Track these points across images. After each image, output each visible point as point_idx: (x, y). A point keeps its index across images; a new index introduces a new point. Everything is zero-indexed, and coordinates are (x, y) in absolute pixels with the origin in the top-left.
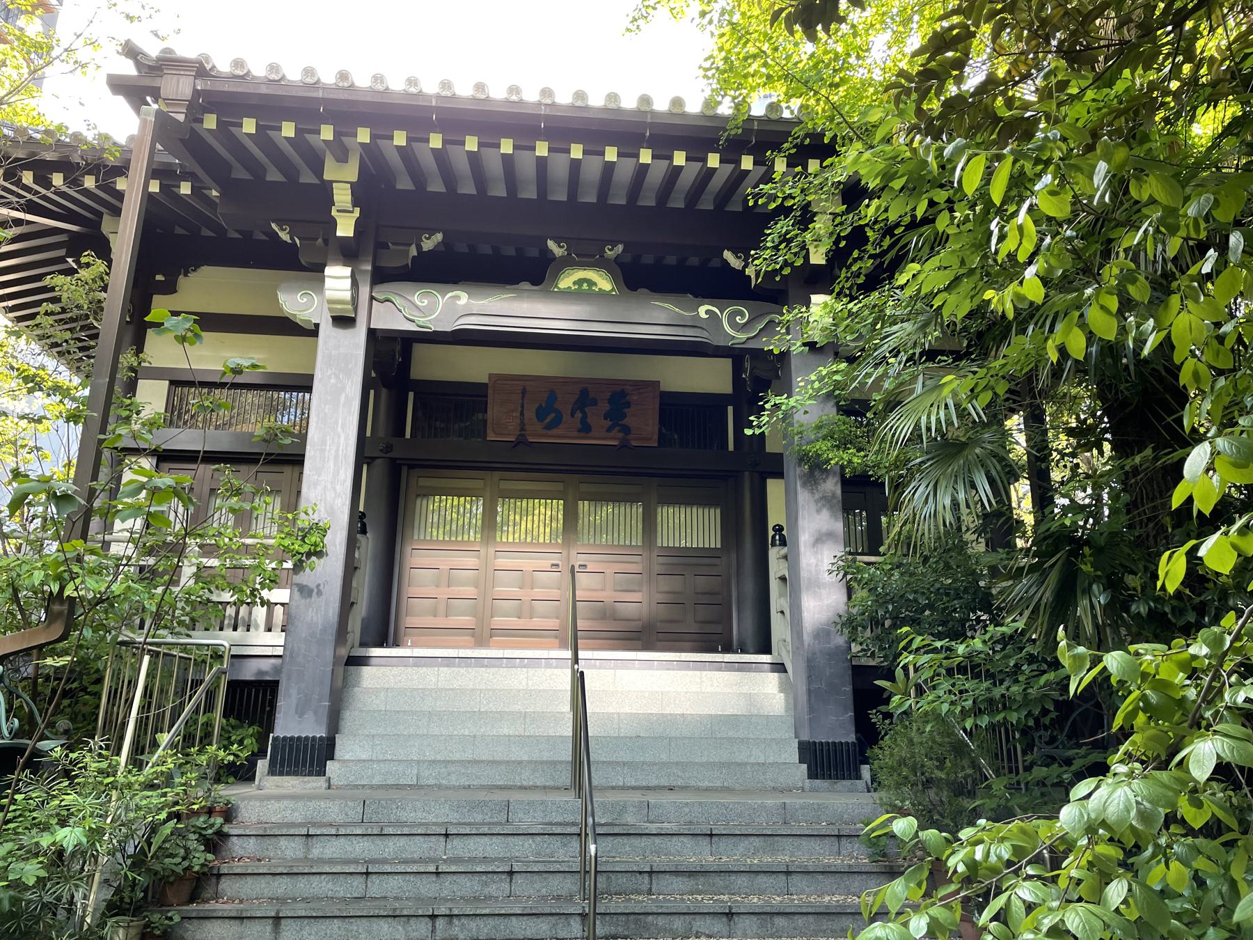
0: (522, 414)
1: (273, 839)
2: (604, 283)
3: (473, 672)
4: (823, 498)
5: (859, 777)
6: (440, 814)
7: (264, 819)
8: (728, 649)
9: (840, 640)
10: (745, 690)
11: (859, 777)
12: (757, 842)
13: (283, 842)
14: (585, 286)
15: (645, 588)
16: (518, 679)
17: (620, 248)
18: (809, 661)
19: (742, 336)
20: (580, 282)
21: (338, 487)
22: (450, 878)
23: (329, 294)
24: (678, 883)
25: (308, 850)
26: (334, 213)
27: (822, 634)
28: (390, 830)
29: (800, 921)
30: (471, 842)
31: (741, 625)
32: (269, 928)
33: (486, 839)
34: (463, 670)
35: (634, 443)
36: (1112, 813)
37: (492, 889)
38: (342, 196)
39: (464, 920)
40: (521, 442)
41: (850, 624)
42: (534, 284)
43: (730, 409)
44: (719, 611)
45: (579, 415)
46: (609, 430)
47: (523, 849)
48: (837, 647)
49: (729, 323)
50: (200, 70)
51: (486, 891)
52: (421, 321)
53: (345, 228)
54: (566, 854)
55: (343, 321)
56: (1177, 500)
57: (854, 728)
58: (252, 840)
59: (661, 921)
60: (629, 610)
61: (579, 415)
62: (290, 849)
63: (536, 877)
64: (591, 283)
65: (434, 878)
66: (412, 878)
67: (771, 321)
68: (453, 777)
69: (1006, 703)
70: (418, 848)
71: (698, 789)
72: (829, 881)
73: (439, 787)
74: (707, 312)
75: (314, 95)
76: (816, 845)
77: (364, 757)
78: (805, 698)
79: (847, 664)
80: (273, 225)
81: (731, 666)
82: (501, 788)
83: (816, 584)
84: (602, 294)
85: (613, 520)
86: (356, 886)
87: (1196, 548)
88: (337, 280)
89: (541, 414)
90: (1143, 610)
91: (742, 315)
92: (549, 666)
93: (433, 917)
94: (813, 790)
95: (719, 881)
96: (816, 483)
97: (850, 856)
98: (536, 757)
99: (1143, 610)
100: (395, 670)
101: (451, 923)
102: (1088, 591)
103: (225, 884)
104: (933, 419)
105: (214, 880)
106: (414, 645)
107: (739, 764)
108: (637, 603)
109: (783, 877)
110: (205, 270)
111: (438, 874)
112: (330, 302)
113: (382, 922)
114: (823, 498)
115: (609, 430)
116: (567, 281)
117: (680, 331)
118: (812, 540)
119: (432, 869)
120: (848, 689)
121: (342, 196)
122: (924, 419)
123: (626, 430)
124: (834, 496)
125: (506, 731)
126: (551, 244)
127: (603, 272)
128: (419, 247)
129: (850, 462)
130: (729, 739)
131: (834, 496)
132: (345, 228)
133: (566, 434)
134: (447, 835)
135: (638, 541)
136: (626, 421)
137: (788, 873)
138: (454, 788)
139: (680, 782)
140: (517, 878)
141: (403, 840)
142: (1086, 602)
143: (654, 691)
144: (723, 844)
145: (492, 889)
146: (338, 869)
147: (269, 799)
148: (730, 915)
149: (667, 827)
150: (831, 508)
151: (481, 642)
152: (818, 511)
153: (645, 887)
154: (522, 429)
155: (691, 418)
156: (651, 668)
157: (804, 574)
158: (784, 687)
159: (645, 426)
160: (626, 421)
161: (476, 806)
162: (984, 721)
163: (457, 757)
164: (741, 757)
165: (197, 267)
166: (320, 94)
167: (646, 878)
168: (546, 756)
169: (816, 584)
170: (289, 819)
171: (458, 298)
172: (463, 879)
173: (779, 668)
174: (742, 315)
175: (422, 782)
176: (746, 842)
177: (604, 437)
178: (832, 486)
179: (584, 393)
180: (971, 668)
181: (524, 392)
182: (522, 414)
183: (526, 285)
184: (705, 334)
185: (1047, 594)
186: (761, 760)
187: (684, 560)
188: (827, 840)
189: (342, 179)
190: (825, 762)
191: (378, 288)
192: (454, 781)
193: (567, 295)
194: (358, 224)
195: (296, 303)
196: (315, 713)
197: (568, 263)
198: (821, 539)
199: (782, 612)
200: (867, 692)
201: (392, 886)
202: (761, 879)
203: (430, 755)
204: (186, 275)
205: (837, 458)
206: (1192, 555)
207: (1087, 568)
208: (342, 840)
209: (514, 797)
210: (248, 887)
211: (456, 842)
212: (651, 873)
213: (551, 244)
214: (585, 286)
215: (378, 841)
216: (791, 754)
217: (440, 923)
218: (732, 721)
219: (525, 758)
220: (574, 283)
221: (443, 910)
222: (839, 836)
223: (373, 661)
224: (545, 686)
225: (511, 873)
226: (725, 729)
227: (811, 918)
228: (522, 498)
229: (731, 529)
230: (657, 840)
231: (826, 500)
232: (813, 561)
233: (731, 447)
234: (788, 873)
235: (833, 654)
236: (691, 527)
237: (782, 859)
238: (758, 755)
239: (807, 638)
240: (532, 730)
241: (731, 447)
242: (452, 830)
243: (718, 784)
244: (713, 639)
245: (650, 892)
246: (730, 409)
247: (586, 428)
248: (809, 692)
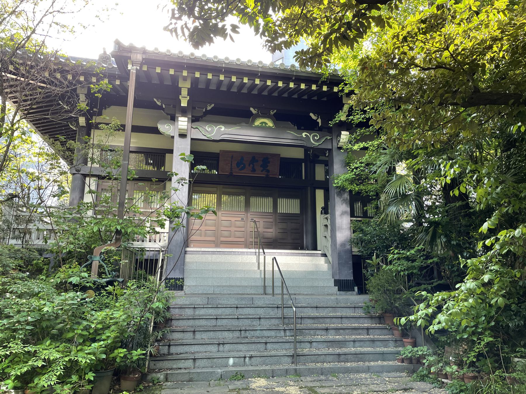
0: (231, 165)
1: (184, 309)
2: (270, 124)
3: (224, 256)
4: (344, 200)
5: (354, 291)
6: (233, 302)
7: (177, 303)
8: (302, 249)
9: (348, 247)
10: (314, 263)
11: (354, 291)
12: (330, 309)
13: (187, 310)
14: (264, 125)
15: (274, 227)
16: (239, 259)
17: (275, 111)
18: (339, 253)
19: (317, 144)
20: (262, 123)
21: (183, 194)
22: (241, 320)
23: (180, 127)
24: (309, 321)
25: (195, 312)
26: (180, 98)
27: (343, 245)
28: (220, 306)
29: (347, 331)
30: (245, 309)
31: (307, 240)
32: (192, 334)
33: (249, 309)
34: (220, 256)
35: (271, 176)
36: (471, 287)
37: (254, 323)
38: (184, 92)
39: (250, 331)
40: (231, 174)
41: (352, 242)
42: (246, 123)
43: (303, 164)
44: (297, 235)
45: (251, 165)
46: (262, 171)
47: (261, 312)
48: (348, 249)
49: (313, 139)
50: (144, 51)
51: (253, 323)
52: (209, 136)
53: (184, 104)
54: (279, 313)
55: (183, 136)
56: (480, 231)
57: (356, 274)
58: (177, 309)
59: (307, 331)
60: (269, 235)
61: (251, 165)
62: (189, 312)
63: (267, 319)
64: (266, 124)
65: (237, 320)
66: (230, 320)
67: (326, 139)
68: (225, 291)
69: (413, 267)
70: (228, 311)
71: (304, 295)
72: (353, 320)
73: (221, 294)
74: (305, 135)
75: (184, 61)
76: (348, 310)
77: (194, 284)
78: (337, 265)
79: (351, 255)
80: (155, 100)
81: (308, 255)
82: (240, 294)
83: (341, 228)
84: (270, 128)
85: (262, 204)
86: (214, 322)
87: (485, 242)
88: (183, 122)
89: (238, 165)
90: (455, 243)
91: (317, 136)
92: (247, 255)
93: (241, 330)
94: (340, 295)
95: (321, 320)
96: (341, 195)
97: (358, 313)
98: (250, 284)
99: (455, 243)
100: (197, 256)
101: (246, 332)
102: (440, 237)
103: (174, 322)
104: (401, 189)
105: (170, 321)
106: (194, 247)
107: (316, 287)
108: (272, 232)
109: (340, 319)
110: (112, 107)
111: (238, 318)
112: (179, 129)
113: (225, 332)
114: (344, 200)
115: (262, 171)
116: (257, 123)
117: (296, 141)
118: (340, 214)
119: (236, 317)
120: (351, 262)
121: (184, 92)
122: (398, 189)
123: (268, 171)
124: (347, 198)
125: (238, 276)
126: (252, 109)
127: (270, 120)
128: (206, 109)
129: (354, 189)
130: (312, 279)
131: (347, 198)
132: (184, 104)
133: (247, 172)
134: (237, 307)
135: (271, 210)
136: (268, 168)
137: (342, 318)
138: (226, 294)
139: (298, 293)
140: (261, 319)
141: (224, 309)
142: (439, 240)
143: (291, 262)
144: (320, 309)
145: (254, 323)
146: (208, 317)
147: (178, 298)
148: (327, 329)
149: (304, 305)
150: (346, 203)
151: (217, 246)
152: (342, 204)
153: (300, 322)
154: (231, 170)
155: (289, 166)
156: (282, 255)
157: (337, 225)
158: (328, 262)
159: (274, 169)
160: (268, 168)
161: (242, 299)
162: (406, 273)
163: (224, 284)
164: (316, 284)
165: (109, 107)
166: (185, 61)
167: (300, 319)
168: (253, 284)
169: (341, 228)
170: (185, 303)
171: (221, 128)
172: (245, 320)
173: (325, 255)
174: (317, 136)
175: (215, 293)
176: (327, 309)
177: (260, 174)
178: (346, 196)
179: (254, 158)
180: (407, 259)
181: (232, 157)
182: (231, 165)
183: (244, 124)
184: (305, 143)
185: (428, 238)
186: (322, 285)
187: (287, 217)
188: (351, 309)
189: (185, 87)
190: (342, 286)
191: (193, 124)
192: (225, 292)
193: (258, 128)
194: (188, 101)
195: (165, 128)
196: (179, 270)
197: (257, 116)
198: (343, 213)
199: (325, 237)
200: (358, 264)
201: (224, 322)
202: (334, 319)
203: (215, 284)
204: (105, 109)
205: (349, 188)
206: (484, 243)
207: (440, 231)
208: (205, 309)
209: (254, 296)
210: (181, 323)
211: (240, 309)
212: (301, 318)
213: (252, 109)
214: (264, 125)
215: (216, 309)
216: (332, 283)
217: (243, 332)
218: (311, 273)
219: (246, 285)
220: (260, 123)
221: (243, 329)
222: (355, 307)
223: (188, 252)
224: (248, 261)
225: (260, 318)
226: (311, 275)
227: (350, 330)
228: (239, 195)
229: (303, 207)
230: (301, 309)
231: (344, 200)
232: (340, 221)
233: (304, 178)
234: (342, 318)
235: (346, 251)
236: (289, 206)
237: (339, 314)
238: (321, 284)
239: (338, 246)
240: (247, 276)
241: (304, 178)
242: (239, 306)
243: (310, 293)
244: (297, 244)
245: (301, 324)
246: (303, 164)
247: (254, 170)
248: (339, 263)
